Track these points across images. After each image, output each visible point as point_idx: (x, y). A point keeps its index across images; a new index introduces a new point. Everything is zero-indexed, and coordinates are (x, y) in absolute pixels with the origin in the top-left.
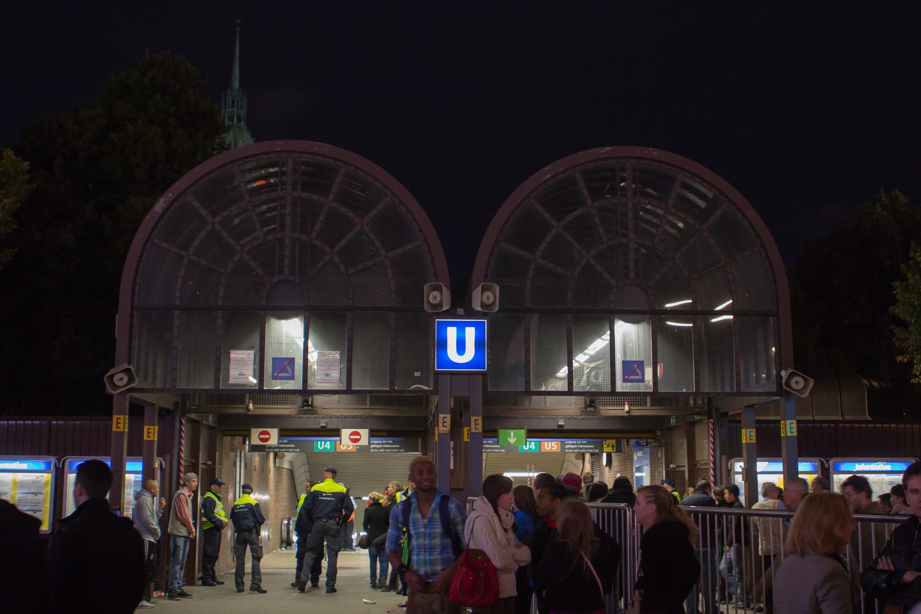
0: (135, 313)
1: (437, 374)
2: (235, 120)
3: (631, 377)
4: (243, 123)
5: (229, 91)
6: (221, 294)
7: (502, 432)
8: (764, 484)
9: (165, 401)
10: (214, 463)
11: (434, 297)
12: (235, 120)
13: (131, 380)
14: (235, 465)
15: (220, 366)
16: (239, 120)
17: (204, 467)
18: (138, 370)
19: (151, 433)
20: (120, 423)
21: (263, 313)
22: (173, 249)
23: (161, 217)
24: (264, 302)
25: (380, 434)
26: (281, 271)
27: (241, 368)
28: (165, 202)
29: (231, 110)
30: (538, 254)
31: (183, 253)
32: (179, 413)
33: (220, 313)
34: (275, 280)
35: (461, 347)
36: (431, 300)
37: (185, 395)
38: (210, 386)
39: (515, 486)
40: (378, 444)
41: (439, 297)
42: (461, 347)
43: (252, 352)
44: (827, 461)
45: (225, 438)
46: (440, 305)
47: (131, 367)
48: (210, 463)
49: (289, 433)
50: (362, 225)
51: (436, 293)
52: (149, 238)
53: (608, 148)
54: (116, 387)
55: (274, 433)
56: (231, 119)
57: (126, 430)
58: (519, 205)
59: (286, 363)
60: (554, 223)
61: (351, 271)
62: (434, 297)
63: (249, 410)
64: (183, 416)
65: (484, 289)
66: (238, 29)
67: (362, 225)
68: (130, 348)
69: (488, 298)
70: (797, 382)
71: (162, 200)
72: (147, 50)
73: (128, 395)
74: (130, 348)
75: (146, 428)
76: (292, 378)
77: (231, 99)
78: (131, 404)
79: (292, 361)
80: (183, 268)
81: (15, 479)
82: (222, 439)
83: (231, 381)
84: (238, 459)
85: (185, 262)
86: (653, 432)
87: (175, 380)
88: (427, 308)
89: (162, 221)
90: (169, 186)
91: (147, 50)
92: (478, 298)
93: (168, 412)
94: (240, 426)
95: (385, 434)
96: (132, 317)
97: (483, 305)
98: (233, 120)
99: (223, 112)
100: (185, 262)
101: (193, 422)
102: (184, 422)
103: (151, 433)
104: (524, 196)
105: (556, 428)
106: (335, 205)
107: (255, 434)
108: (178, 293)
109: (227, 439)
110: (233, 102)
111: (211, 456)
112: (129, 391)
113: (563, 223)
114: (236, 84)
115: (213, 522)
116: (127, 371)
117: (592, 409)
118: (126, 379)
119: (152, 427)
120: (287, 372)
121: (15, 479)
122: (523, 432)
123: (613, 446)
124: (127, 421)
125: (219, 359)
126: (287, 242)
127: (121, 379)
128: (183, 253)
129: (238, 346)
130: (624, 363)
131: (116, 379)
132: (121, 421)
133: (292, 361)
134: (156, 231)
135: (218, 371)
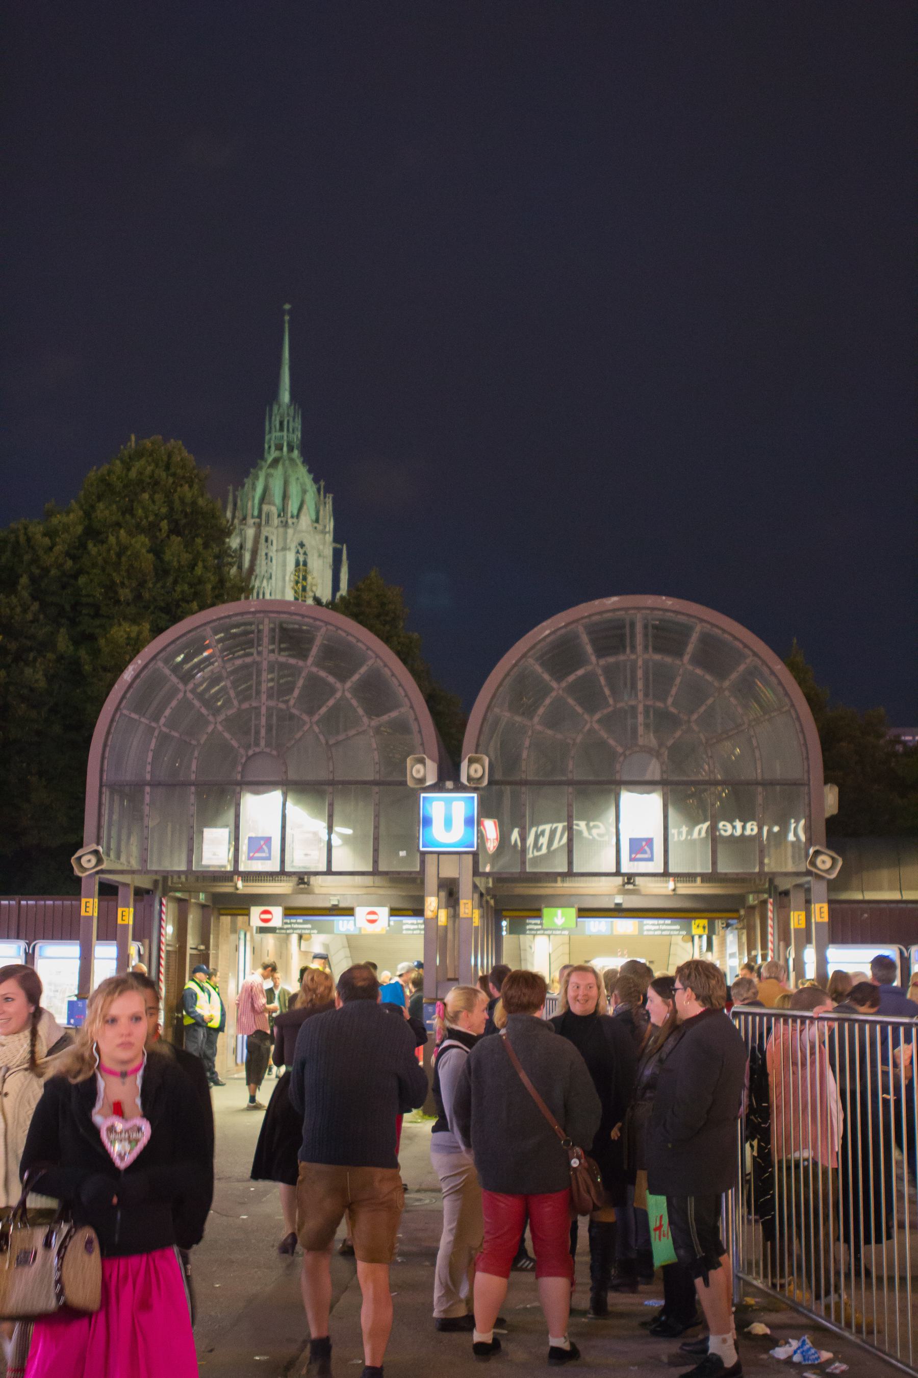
0: (104, 789)
1: (423, 854)
2: (285, 449)
3: (639, 856)
4: (296, 453)
5: (275, 408)
6: (194, 768)
7: (546, 911)
8: (605, 973)
9: (144, 882)
10: (208, 948)
11: (416, 771)
12: (285, 449)
13: (100, 861)
14: (237, 949)
15: (192, 845)
16: (291, 449)
17: (194, 952)
18: (109, 849)
19: (126, 916)
20: (90, 906)
21: (238, 789)
22: (143, 720)
23: (130, 686)
24: (239, 777)
25: (404, 913)
26: (257, 744)
27: (215, 848)
28: (134, 670)
29: (278, 434)
30: (536, 719)
31: (153, 724)
32: (158, 893)
33: (193, 789)
34: (250, 753)
35: (448, 823)
36: (414, 774)
37: (166, 876)
38: (183, 868)
39: (855, 982)
40: (413, 924)
41: (427, 771)
42: (448, 823)
44: (907, 950)
45: (223, 918)
46: (422, 780)
47: (100, 849)
48: (202, 947)
49: (304, 912)
50: (344, 691)
51: (419, 766)
52: (118, 708)
54: (85, 870)
55: (277, 912)
56: (279, 448)
57: (96, 914)
58: (515, 665)
59: (262, 842)
60: (554, 684)
61: (331, 742)
62: (416, 771)
63: (237, 889)
64: (164, 894)
65: (471, 761)
66: (287, 318)
67: (344, 691)
68: (99, 827)
69: (476, 771)
70: (824, 862)
72: (133, 438)
73: (97, 877)
74: (99, 827)
75: (120, 910)
76: (269, 858)
77: (278, 419)
78: (102, 885)
79: (268, 840)
80: (154, 740)
82: (218, 919)
83: (205, 862)
84: (242, 942)
85: (156, 734)
86: (737, 911)
87: (146, 861)
88: (410, 783)
89: (131, 690)
90: (138, 652)
91: (133, 438)
92: (466, 771)
93: (148, 892)
94: (239, 905)
95: (410, 913)
96: (101, 793)
97: (469, 779)
99: (267, 438)
100: (156, 734)
101: (180, 900)
102: (164, 902)
103: (126, 916)
104: (524, 653)
105: (612, 906)
106: (314, 669)
107: (256, 911)
108: (149, 768)
109: (226, 920)
110: (281, 423)
111: (204, 939)
112: (97, 873)
113: (564, 684)
114: (285, 397)
115: (193, 1018)
116: (96, 852)
117: (630, 887)
118: (94, 861)
119: (126, 909)
120: (264, 852)
122: (573, 912)
123: (704, 927)
124: (97, 905)
125: (192, 839)
126: (263, 710)
127: (89, 861)
128: (153, 724)
129: (211, 823)
131: (84, 861)
132: (90, 905)
133: (268, 840)
134: (125, 701)
135: (191, 851)
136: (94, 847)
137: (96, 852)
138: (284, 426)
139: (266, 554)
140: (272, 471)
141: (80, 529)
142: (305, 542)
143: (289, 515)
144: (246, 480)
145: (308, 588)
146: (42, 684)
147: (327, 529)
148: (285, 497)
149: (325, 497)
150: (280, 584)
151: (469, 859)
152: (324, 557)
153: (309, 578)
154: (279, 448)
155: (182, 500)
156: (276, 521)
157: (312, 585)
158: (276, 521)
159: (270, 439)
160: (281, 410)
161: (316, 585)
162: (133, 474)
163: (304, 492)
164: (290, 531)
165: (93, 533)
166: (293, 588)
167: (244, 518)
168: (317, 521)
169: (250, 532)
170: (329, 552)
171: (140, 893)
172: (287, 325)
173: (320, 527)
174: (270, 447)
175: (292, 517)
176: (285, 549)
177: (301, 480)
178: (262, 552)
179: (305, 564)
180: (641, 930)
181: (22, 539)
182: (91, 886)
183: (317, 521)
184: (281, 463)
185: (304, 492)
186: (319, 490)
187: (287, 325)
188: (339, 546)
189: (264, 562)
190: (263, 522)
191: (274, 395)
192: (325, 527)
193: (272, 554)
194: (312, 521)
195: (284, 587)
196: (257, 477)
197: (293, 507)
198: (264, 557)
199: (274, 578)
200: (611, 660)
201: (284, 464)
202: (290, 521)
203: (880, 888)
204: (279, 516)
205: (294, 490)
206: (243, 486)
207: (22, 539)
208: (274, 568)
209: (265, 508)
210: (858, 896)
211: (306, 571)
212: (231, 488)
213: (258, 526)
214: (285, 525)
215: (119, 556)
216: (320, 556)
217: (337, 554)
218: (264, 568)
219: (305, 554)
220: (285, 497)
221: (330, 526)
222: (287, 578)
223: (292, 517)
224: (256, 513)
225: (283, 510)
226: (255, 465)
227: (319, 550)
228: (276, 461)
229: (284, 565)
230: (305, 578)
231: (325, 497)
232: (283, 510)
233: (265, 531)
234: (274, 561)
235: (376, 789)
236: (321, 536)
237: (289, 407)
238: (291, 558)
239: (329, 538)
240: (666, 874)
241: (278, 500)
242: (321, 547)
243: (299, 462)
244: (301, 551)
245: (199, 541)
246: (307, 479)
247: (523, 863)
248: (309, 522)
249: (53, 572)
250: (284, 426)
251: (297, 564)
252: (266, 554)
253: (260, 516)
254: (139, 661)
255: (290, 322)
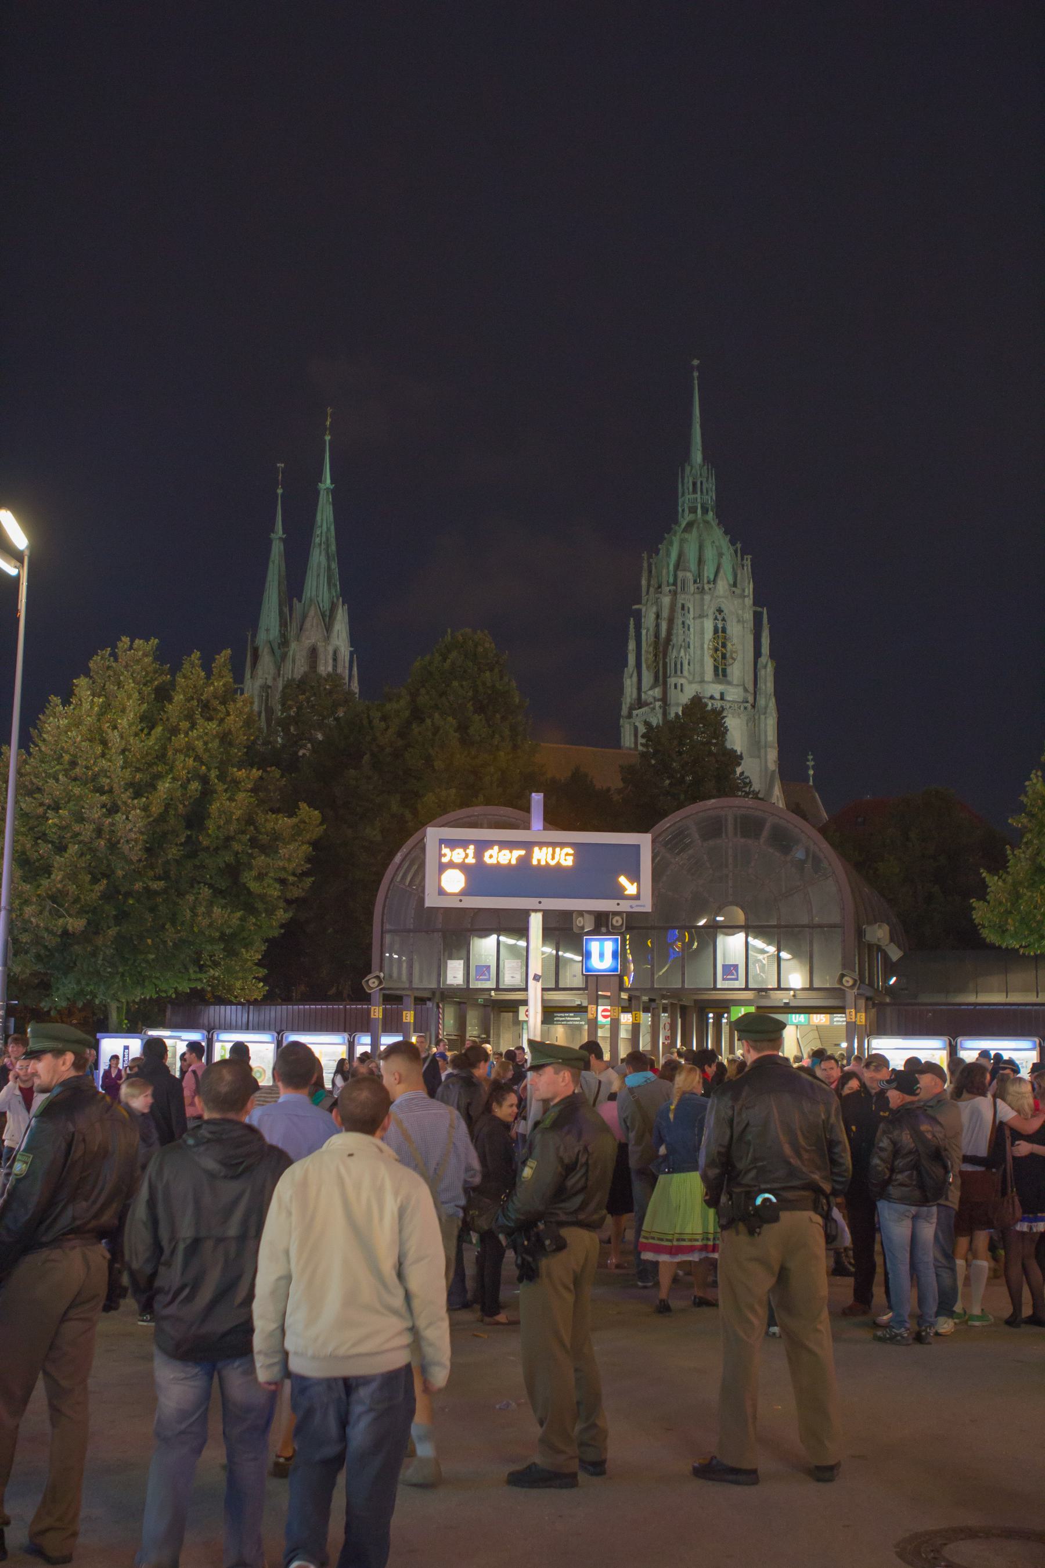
2: (699, 511)
4: (711, 514)
5: (688, 469)
12: (699, 511)
13: (380, 983)
15: (441, 971)
16: (705, 511)
27: (455, 973)
35: (602, 955)
42: (602, 955)
43: (462, 962)
46: (583, 928)
47: (382, 975)
53: (713, 801)
56: (693, 510)
66: (696, 374)
71: (399, 854)
79: (488, 967)
81: (1041, 1227)
83: (449, 982)
88: (575, 930)
91: (449, 631)
98: (695, 512)
99: (680, 501)
110: (694, 484)
112: (381, 989)
114: (697, 456)
116: (378, 977)
118: (377, 983)
121: (1041, 1227)
130: (724, 966)
135: (439, 975)
136: (377, 973)
137: (378, 977)
138: (697, 486)
139: (683, 623)
140: (686, 535)
141: (407, 713)
142: (723, 607)
143: (705, 581)
144: (660, 546)
145: (728, 655)
146: (379, 838)
147: (746, 593)
148: (700, 561)
149: (742, 559)
150: (699, 652)
151: (617, 979)
152: (743, 622)
153: (729, 645)
154: (693, 510)
155: (484, 684)
156: (692, 588)
157: (732, 652)
158: (692, 588)
159: (684, 502)
160: (694, 471)
161: (736, 652)
162: (447, 665)
163: (721, 555)
164: (707, 597)
165: (417, 715)
166: (712, 656)
167: (660, 587)
168: (735, 585)
169: (666, 600)
170: (749, 616)
171: (420, 1001)
172: (696, 382)
173: (738, 591)
174: (683, 510)
175: (709, 582)
176: (701, 616)
177: (717, 544)
178: (678, 621)
179: (724, 630)
180: (832, 1021)
181: (365, 722)
182: (377, 997)
183: (735, 585)
184: (695, 526)
185: (721, 555)
186: (736, 552)
187: (696, 382)
188: (759, 609)
189: (681, 632)
190: (679, 590)
191: (686, 456)
192: (744, 591)
193: (690, 622)
194: (730, 585)
195: (703, 655)
196: (671, 543)
197: (709, 571)
198: (680, 626)
199: (692, 646)
200: (711, 843)
201: (698, 528)
202: (706, 587)
203: (989, 990)
204: (695, 582)
205: (710, 553)
206: (657, 552)
207: (365, 722)
208: (692, 636)
209: (680, 574)
210: (972, 999)
211: (725, 638)
212: (645, 555)
213: (674, 593)
214: (702, 591)
215: (435, 734)
216: (739, 621)
217: (757, 618)
218: (681, 638)
219: (724, 620)
220: (700, 561)
221: (749, 589)
222: (706, 646)
223: (709, 582)
224: (671, 580)
225: (698, 577)
226: (669, 530)
227: (738, 616)
228: (690, 525)
229: (702, 633)
230: (724, 646)
231: (742, 559)
232: (698, 577)
233: (681, 599)
234: (692, 630)
235: (557, 933)
236: (740, 600)
237: (701, 467)
238: (709, 625)
239: (749, 601)
240: (747, 989)
241: (693, 566)
242: (740, 612)
243: (714, 523)
244: (719, 617)
245: (498, 716)
246: (724, 542)
247: (653, 982)
248: (727, 587)
249: (388, 750)
250: (697, 486)
251: (716, 631)
252: (683, 623)
253: (675, 584)
254: (404, 850)
255: (698, 378)
